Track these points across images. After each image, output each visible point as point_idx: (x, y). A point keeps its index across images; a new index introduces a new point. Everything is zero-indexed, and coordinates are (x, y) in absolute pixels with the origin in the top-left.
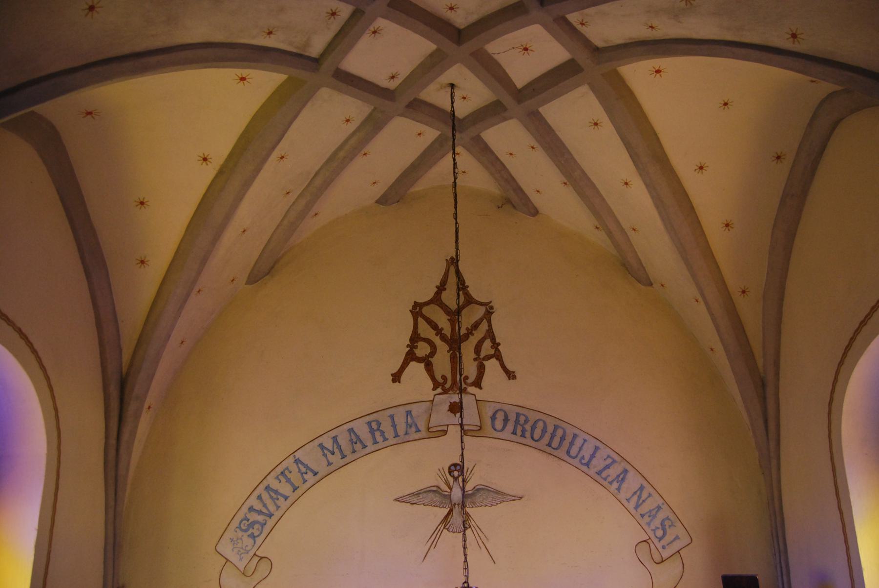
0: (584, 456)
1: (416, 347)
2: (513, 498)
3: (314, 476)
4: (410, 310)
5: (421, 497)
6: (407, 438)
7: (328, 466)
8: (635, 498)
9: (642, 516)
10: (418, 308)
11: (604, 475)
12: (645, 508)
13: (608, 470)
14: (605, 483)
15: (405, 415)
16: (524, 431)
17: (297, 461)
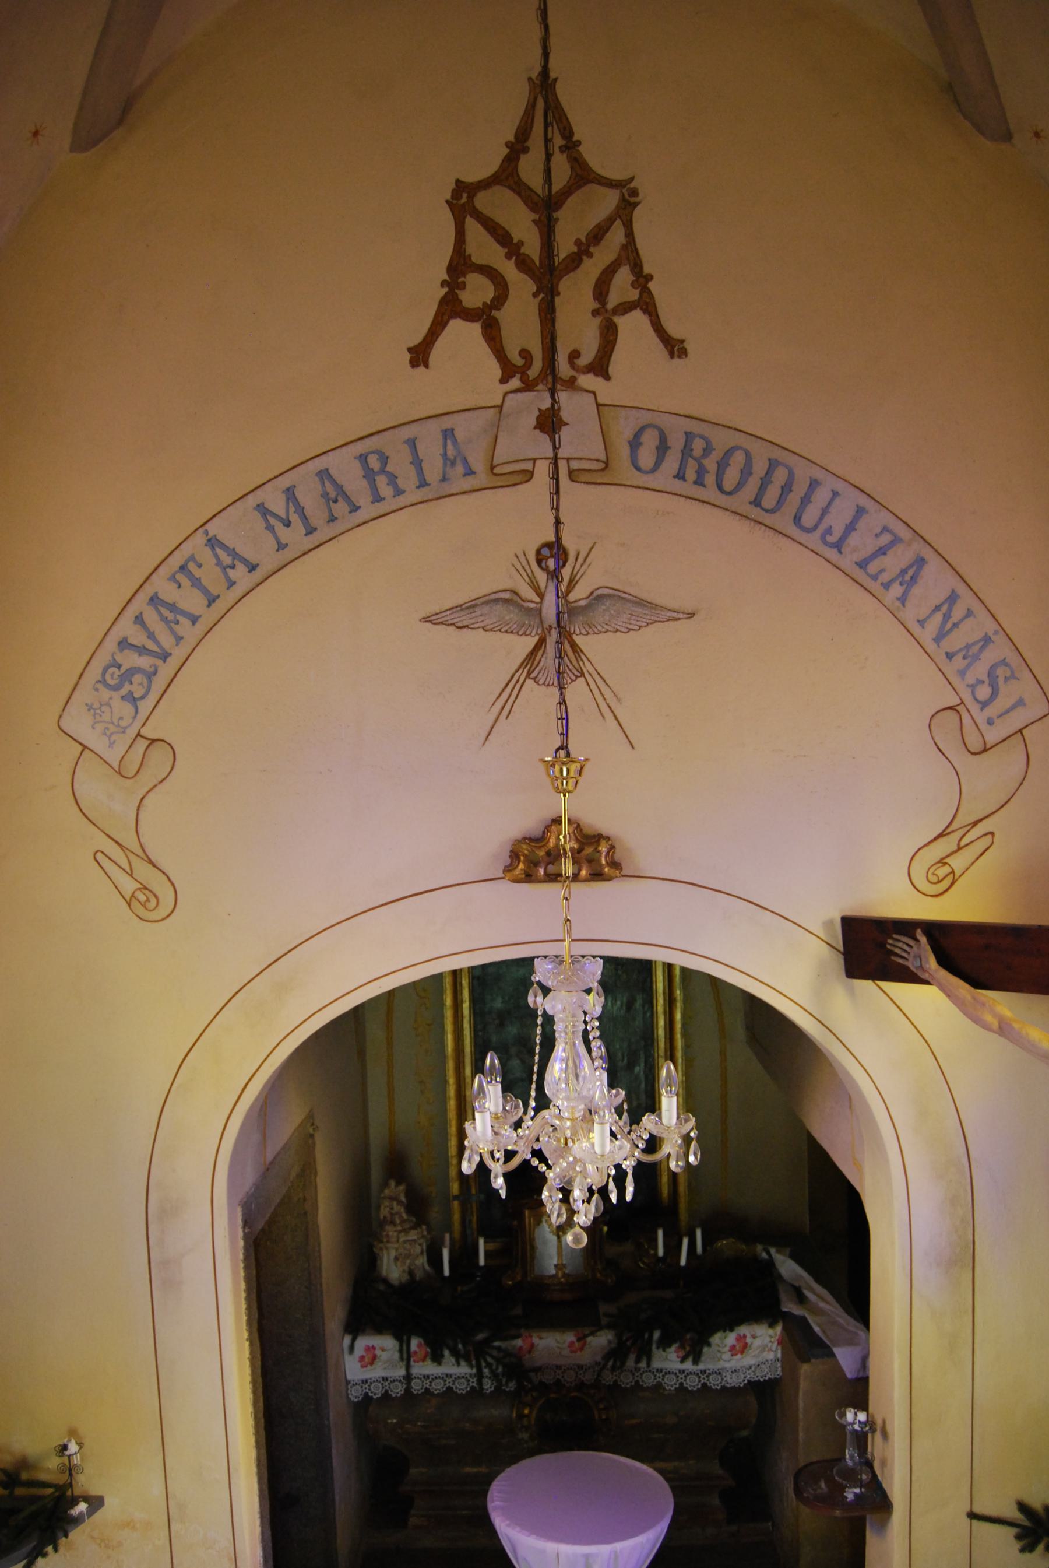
0: (831, 527)
1: (463, 286)
2: (675, 615)
3: (250, 572)
4: (447, 201)
5: (478, 613)
6: (447, 488)
7: (278, 550)
8: (938, 617)
9: (950, 656)
10: (465, 195)
11: (873, 567)
12: (956, 641)
13: (882, 557)
14: (875, 587)
15: (440, 437)
16: (701, 472)
17: (213, 543)
